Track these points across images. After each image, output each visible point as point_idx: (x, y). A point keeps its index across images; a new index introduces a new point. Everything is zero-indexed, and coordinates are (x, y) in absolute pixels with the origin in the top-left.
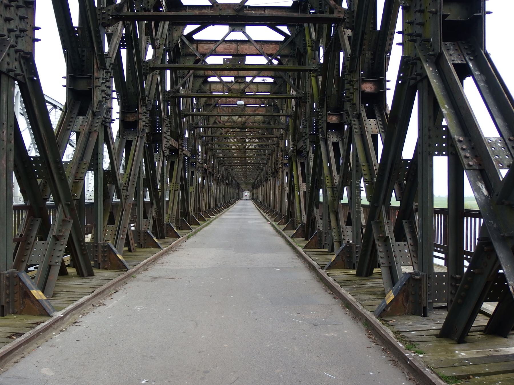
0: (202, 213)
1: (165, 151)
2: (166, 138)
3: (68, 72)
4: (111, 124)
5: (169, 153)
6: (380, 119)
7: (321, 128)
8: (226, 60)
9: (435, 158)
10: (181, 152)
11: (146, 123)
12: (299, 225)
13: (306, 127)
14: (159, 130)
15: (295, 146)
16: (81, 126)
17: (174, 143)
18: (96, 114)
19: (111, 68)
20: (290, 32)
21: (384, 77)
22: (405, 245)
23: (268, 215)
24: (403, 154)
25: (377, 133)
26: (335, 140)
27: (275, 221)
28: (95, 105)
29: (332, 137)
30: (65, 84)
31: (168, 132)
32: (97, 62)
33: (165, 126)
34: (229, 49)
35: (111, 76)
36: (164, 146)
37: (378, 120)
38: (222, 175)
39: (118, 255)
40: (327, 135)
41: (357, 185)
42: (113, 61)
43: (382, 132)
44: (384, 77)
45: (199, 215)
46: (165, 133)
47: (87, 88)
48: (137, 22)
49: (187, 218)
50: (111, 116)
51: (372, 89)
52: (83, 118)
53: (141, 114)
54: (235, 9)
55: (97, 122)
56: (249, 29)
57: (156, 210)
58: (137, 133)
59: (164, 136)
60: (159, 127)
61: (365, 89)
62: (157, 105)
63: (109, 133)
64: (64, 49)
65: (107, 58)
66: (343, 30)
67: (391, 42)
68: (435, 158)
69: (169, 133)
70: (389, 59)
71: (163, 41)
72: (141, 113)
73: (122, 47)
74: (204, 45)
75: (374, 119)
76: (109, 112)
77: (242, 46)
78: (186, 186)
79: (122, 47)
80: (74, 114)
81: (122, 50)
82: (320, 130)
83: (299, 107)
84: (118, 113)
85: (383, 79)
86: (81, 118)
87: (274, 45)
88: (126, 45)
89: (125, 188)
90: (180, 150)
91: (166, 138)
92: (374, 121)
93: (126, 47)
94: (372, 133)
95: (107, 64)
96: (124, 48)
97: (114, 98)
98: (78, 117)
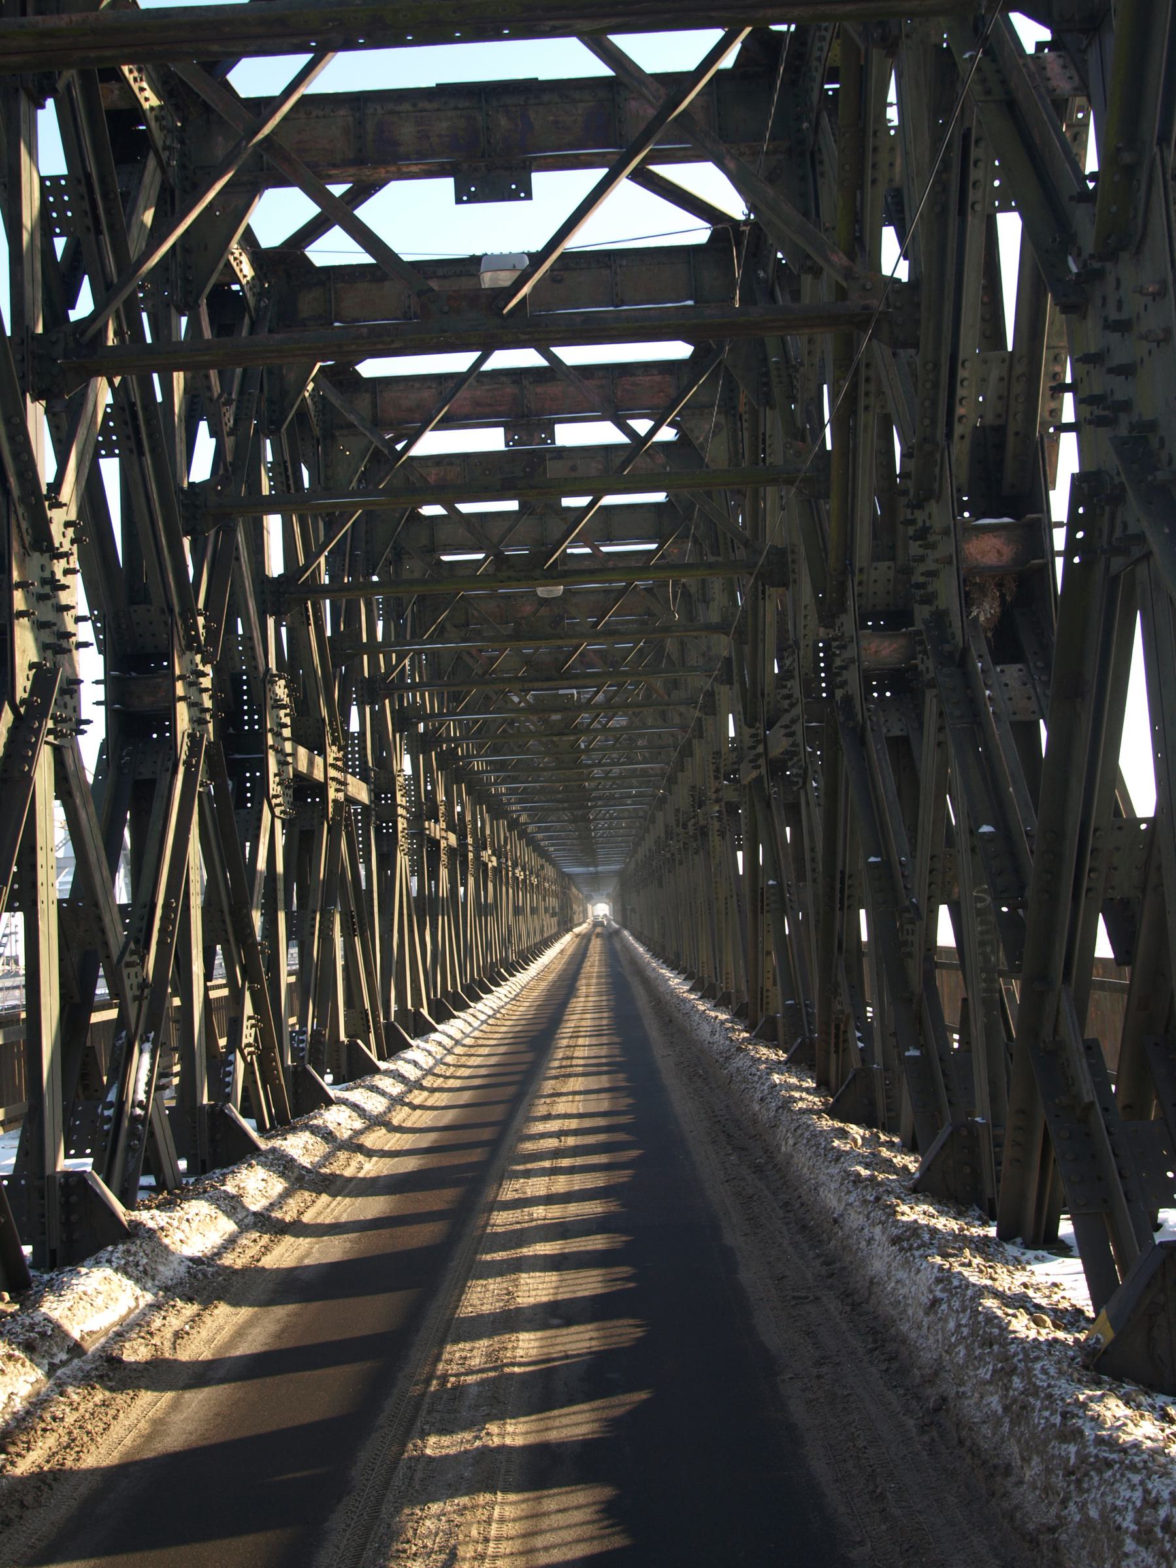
4: (80, 737)
6: (1040, 664)
8: (522, 195)
13: (793, 677)
15: (758, 742)
19: (68, 539)
21: (1041, 511)
23: (683, 977)
25: (1032, 717)
26: (896, 732)
29: (883, 720)
32: (19, 526)
35: (72, 566)
41: (979, 905)
42: (73, 516)
44: (1041, 511)
48: (155, 376)
49: (372, 1036)
50: (76, 709)
60: (250, 713)
61: (979, 557)
62: (240, 631)
71: (910, 932)
73: (103, 452)
74: (399, 394)
75: (1020, 666)
77: (539, 390)
79: (103, 452)
81: (102, 462)
83: (764, 599)
84: (98, 703)
85: (1039, 520)
87: (658, 378)
88: (116, 444)
89: (135, 958)
90: (332, 786)
92: (1020, 670)
93: (117, 451)
94: (1017, 718)
95: (56, 529)
96: (110, 455)
97: (86, 645)
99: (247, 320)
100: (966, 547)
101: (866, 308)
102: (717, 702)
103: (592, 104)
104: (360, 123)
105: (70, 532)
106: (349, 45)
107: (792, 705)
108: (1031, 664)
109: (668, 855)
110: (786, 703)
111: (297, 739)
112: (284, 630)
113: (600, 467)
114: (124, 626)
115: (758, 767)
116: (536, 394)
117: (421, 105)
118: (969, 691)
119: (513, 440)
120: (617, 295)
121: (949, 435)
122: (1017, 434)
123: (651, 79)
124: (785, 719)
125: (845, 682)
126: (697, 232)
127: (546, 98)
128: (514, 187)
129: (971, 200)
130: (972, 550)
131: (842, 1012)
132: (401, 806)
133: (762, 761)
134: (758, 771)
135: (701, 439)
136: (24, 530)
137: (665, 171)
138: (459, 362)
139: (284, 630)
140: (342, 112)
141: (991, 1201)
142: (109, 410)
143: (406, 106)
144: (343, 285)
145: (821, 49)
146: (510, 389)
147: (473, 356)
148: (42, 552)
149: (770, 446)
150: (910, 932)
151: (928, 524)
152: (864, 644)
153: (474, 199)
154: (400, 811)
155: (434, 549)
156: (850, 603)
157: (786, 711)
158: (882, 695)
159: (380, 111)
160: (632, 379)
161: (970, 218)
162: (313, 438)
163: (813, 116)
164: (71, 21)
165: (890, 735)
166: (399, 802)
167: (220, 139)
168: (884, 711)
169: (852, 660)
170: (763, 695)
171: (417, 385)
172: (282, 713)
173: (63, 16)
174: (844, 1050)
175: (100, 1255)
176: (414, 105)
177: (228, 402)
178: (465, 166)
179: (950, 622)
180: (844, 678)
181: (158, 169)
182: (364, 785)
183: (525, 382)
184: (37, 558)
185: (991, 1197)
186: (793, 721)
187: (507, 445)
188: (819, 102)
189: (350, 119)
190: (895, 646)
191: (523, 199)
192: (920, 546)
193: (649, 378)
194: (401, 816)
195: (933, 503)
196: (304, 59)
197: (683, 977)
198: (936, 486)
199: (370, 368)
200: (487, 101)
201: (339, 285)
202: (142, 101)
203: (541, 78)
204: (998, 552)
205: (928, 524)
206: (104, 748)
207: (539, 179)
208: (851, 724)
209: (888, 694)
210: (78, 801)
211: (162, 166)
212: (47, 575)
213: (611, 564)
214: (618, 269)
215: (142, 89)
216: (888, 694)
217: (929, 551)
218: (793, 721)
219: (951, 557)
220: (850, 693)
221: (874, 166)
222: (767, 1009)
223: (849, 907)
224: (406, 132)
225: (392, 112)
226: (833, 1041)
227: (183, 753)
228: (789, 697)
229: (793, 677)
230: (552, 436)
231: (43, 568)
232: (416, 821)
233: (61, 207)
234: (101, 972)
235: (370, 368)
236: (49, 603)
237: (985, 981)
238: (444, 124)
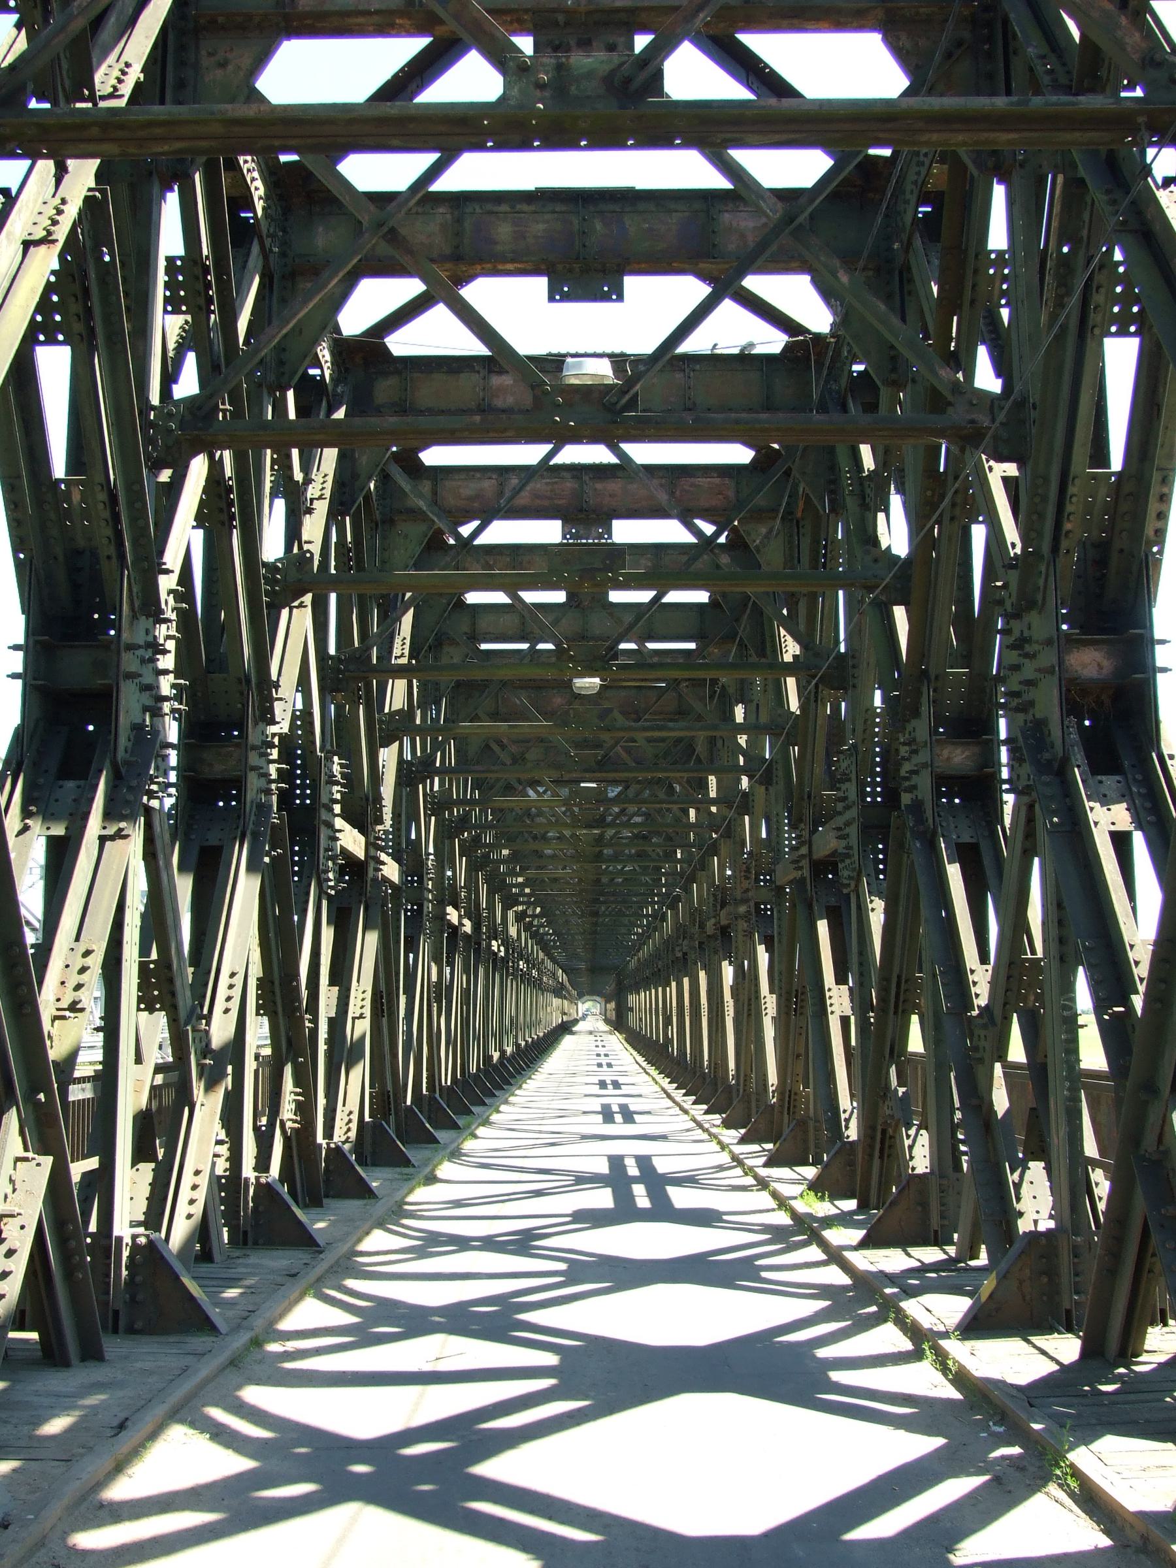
3: (29, 632)
6: (1139, 777)
8: (614, 297)
9: (1108, 342)
14: (303, 796)
18: (123, 770)
21: (1144, 627)
22: (987, 971)
26: (966, 838)
27: (727, 1124)
28: (123, 742)
29: (953, 826)
30: (20, 669)
34: (550, 498)
36: (321, 856)
37: (1130, 781)
38: (506, 942)
39: (187, 1281)
40: (937, 819)
41: (1065, 1013)
43: (1149, 822)
45: (430, 1104)
51: (1105, 671)
52: (79, 787)
53: (129, 682)
57: (293, 1097)
58: (239, 817)
59: (324, 818)
61: (1079, 669)
63: (159, 830)
64: (16, 551)
66: (986, 466)
67: (1163, 507)
68: (1108, 342)
70: (1158, 563)
71: (982, 1037)
74: (459, 483)
75: (1118, 778)
77: (599, 486)
78: (389, 994)
80: (46, 771)
82: (906, 799)
83: (816, 701)
86: (70, 784)
87: (717, 481)
92: (1119, 782)
94: (1113, 828)
98: (61, 782)
99: (324, 404)
100: (1067, 658)
101: (972, 422)
102: (751, 804)
103: (687, 214)
104: (459, 221)
106: (480, 147)
107: (847, 808)
108: (1130, 776)
109: (679, 955)
110: (840, 806)
111: (346, 816)
113: (649, 564)
114: (199, 694)
115: (801, 868)
116: (596, 489)
117: (518, 207)
118: (1067, 800)
119: (570, 533)
120: (689, 399)
121: (1055, 549)
122: (1121, 551)
123: (768, 194)
124: (839, 821)
125: (915, 787)
127: (641, 206)
128: (606, 289)
129: (1091, 323)
130: (1073, 661)
131: (892, 1117)
133: (805, 863)
134: (800, 873)
135: (758, 541)
136: (135, 594)
138: (528, 454)
140: (441, 210)
141: (1068, 1312)
143: (504, 208)
144: (419, 375)
145: (918, 173)
146: (570, 484)
147: (546, 448)
148: (148, 616)
149: (831, 552)
150: (982, 1037)
151: (1026, 634)
152: (937, 750)
153: (566, 298)
155: (476, 637)
156: (924, 709)
157: (840, 813)
158: (950, 801)
159: (478, 210)
160: (692, 480)
161: (1089, 341)
162: (372, 521)
163: (905, 237)
164: (260, 111)
165: (960, 841)
167: (321, 229)
168: (954, 817)
169: (925, 765)
170: (809, 797)
171: (478, 475)
172: (336, 788)
173: (252, 106)
174: (889, 1156)
176: (513, 207)
178: (560, 267)
179: (1049, 731)
180: (913, 783)
181: (261, 257)
183: (586, 478)
184: (144, 622)
185: (1068, 1307)
186: (848, 824)
187: (564, 537)
188: (912, 224)
189: (449, 216)
190: (967, 753)
192: (1020, 655)
193: (709, 479)
195: (1034, 613)
196: (431, 158)
198: (1039, 597)
199: (434, 456)
200: (583, 207)
201: (415, 375)
202: (253, 189)
203: (638, 187)
204: (1099, 665)
205: (1026, 634)
207: (631, 283)
208: (921, 828)
209: (957, 801)
210: (161, 863)
211: (265, 253)
212: (150, 639)
213: (655, 660)
214: (692, 374)
215: (253, 179)
216: (957, 801)
217: (1027, 661)
218: (848, 824)
219: (1053, 667)
220: (919, 798)
221: (974, 286)
222: (794, 1113)
223: (903, 1011)
224: (504, 231)
225: (491, 213)
226: (878, 1146)
227: (251, 822)
228: (844, 799)
229: (849, 780)
231: (147, 632)
232: (441, 903)
235: (434, 456)
236: (151, 665)
237: (1069, 1089)
238: (541, 227)
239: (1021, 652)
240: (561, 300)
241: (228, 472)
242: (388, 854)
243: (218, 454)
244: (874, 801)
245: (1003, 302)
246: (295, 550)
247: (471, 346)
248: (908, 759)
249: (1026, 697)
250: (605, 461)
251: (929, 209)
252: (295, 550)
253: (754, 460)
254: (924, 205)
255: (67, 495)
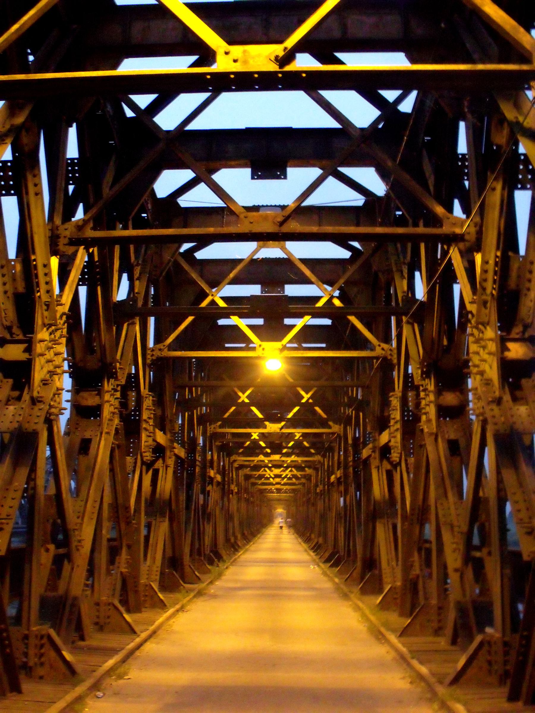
0: (204, 558)
1: (144, 452)
2: (146, 429)
4: (60, 416)
5: (152, 457)
7: (426, 413)
10: (171, 451)
11: (115, 408)
12: (387, 588)
16: (11, 422)
17: (161, 438)
20: (361, 246)
23: (316, 553)
24: (130, 59)
31: (149, 418)
33: (146, 409)
46: (145, 420)
47: (24, 357)
52: (15, 408)
54: (276, 222)
55: (38, 416)
56: (291, 245)
65: (58, 305)
69: (151, 422)
72: (108, 392)
76: (56, 396)
91: (146, 429)
98: (7, 407)
105: (64, 318)
107: (396, 422)
112: (152, 373)
126: (358, 200)
132: (198, 461)
137: (345, 170)
139: (152, 373)
142: (85, 264)
153: (260, 177)
154: (198, 463)
166: (197, 458)
175: (18, 662)
177: (138, 265)
182: (183, 450)
187: (262, 293)
191: (283, 179)
194: (198, 465)
197: (316, 553)
203: (294, 127)
206: (69, 420)
207: (291, 171)
230: (283, 290)
232: (204, 468)
233: (73, 172)
234: (521, 616)
239: (479, 345)
240: (257, 179)
241: (96, 259)
242: (179, 444)
243: (91, 250)
244: (135, 419)
245: (466, 178)
246: (132, 296)
247: (216, 202)
248: (424, 399)
249: (481, 368)
250: (282, 257)
251: (430, 138)
252: (132, 296)
253: (351, 256)
254: (427, 136)
255: (14, 267)
